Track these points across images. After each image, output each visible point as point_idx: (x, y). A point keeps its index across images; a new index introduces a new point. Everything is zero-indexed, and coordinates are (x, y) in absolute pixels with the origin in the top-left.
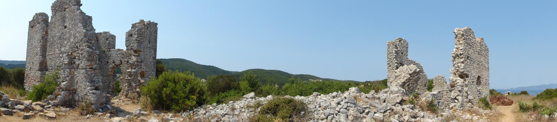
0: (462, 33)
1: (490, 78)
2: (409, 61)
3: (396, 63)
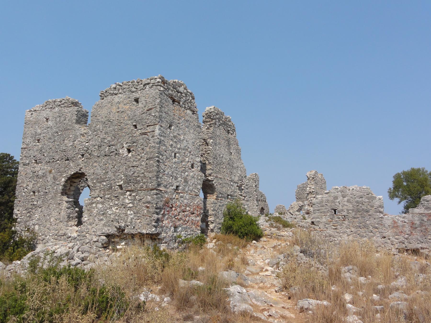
0: (313, 177)
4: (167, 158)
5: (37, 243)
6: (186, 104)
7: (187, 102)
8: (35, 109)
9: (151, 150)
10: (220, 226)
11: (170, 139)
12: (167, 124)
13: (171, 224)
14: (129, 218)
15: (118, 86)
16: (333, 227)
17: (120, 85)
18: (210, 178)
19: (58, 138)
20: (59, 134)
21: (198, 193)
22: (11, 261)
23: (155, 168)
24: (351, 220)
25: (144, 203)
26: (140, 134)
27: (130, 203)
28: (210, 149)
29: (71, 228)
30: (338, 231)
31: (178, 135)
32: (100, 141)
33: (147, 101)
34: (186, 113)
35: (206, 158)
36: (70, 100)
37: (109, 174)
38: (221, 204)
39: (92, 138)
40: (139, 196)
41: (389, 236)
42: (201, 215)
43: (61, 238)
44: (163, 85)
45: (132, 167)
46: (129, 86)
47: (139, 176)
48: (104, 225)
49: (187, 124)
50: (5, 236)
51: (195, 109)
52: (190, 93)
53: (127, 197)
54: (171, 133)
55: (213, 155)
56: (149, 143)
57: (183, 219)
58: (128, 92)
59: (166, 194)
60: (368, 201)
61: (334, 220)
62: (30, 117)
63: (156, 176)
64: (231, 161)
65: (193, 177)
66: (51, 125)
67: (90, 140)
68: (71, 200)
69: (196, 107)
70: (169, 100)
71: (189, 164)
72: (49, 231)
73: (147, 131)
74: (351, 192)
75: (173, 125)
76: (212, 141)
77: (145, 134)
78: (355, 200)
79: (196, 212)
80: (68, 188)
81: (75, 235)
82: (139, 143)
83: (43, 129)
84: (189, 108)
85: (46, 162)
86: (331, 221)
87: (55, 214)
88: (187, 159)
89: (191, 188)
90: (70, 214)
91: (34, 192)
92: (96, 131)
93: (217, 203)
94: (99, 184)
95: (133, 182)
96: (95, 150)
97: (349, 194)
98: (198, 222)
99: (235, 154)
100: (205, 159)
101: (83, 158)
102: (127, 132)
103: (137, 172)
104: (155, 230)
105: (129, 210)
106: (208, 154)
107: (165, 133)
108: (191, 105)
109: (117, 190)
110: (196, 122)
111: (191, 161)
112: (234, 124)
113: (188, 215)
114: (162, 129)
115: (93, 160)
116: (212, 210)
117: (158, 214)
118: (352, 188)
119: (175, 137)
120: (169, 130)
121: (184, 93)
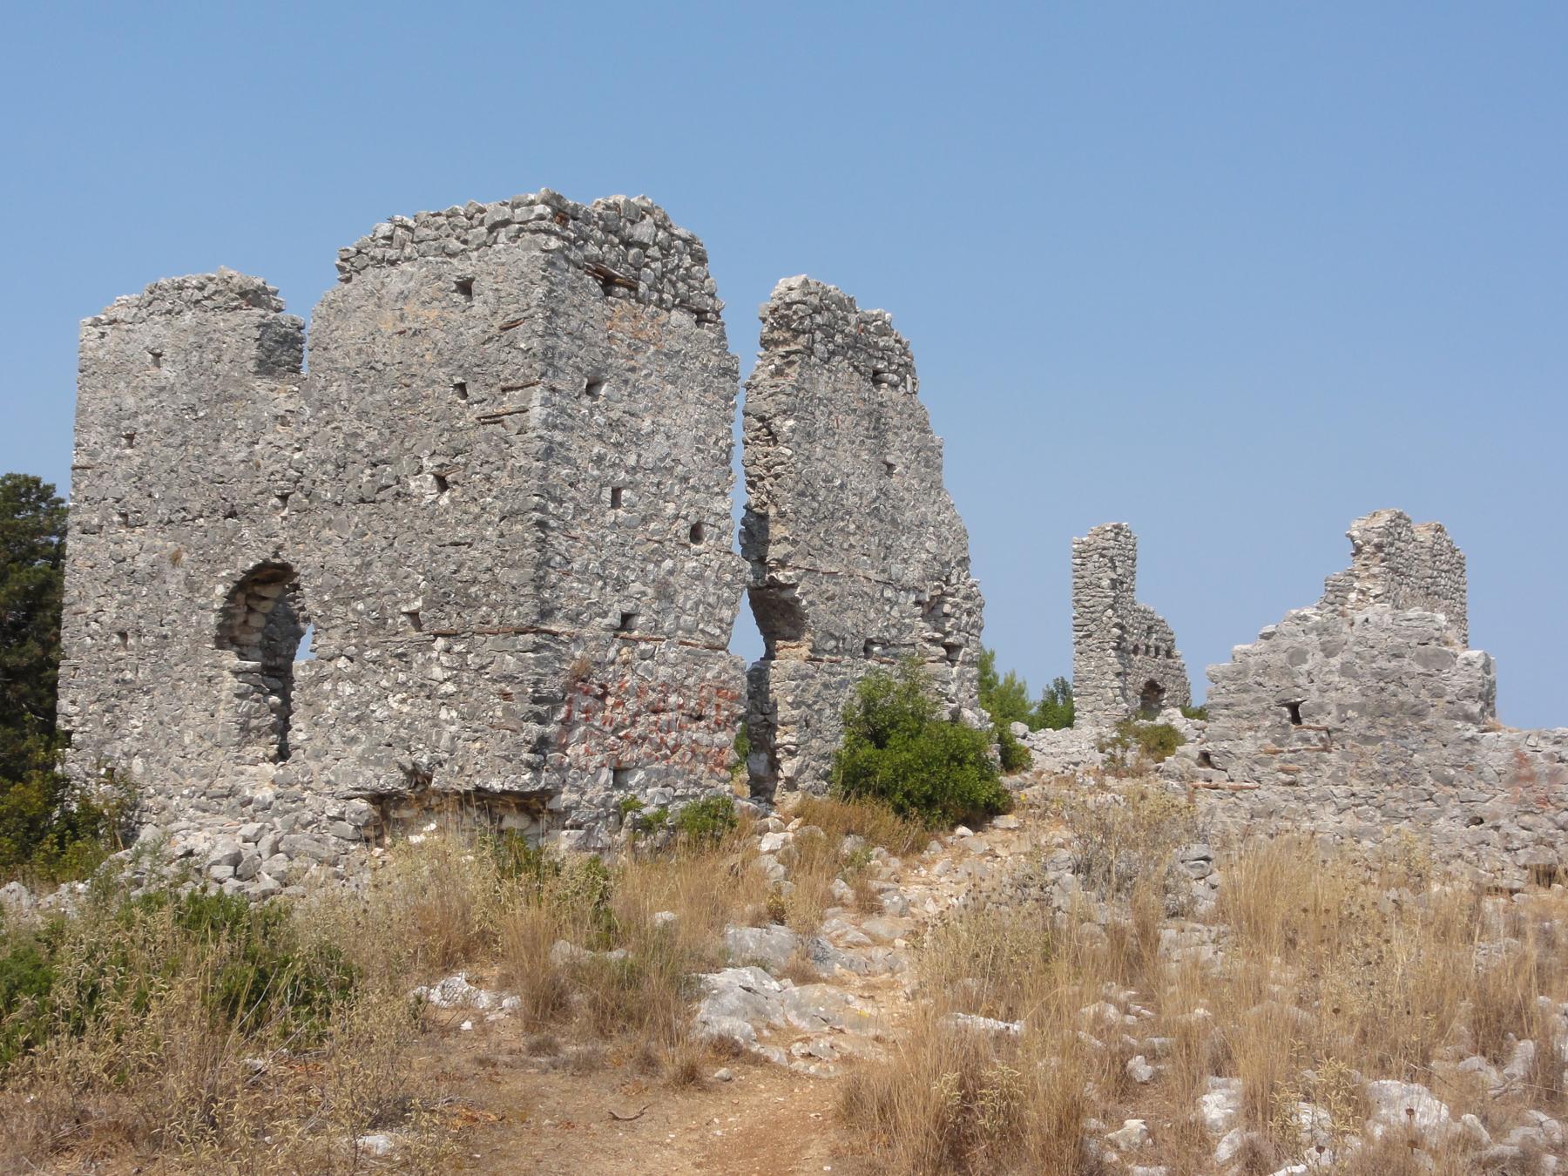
0: (1376, 540)
1: (1499, 704)
2: (1139, 611)
3: (1116, 625)
4: (579, 510)
5: (141, 824)
6: (667, 286)
7: (670, 281)
8: (112, 315)
9: (516, 482)
10: (828, 767)
11: (592, 435)
12: (577, 380)
13: (599, 758)
14: (446, 736)
15: (399, 232)
16: (1283, 776)
17: (407, 228)
18: (781, 576)
19: (198, 430)
20: (201, 414)
21: (724, 638)
22: (54, 882)
23: (530, 550)
24: (1354, 750)
25: (494, 681)
26: (479, 419)
27: (448, 679)
28: (785, 459)
29: (252, 769)
30: (1300, 791)
31: (627, 417)
32: (340, 443)
33: (503, 294)
34: (664, 325)
35: (769, 492)
36: (235, 281)
37: (373, 572)
38: (833, 680)
39: (315, 433)
40: (477, 655)
41: (1496, 816)
42: (734, 723)
43: (220, 804)
44: (557, 228)
45: (451, 544)
46: (437, 229)
47: (475, 581)
48: (363, 760)
49: (668, 370)
50: (31, 796)
51: (710, 301)
52: (685, 241)
53: (438, 659)
54: (597, 413)
55: (797, 483)
56: (507, 454)
57: (651, 740)
58: (435, 256)
59: (578, 648)
60: (1422, 670)
61: (1285, 749)
62: (98, 348)
63: (533, 580)
64: (888, 499)
65: (699, 577)
66: (172, 381)
67: (307, 440)
68: (250, 664)
69: (712, 295)
70: (585, 281)
71: (682, 528)
72: (180, 780)
73: (500, 410)
74: (1357, 633)
75: (607, 380)
76: (791, 423)
77: (495, 419)
78: (1374, 665)
79: (713, 713)
80: (240, 619)
81: (266, 793)
82: (476, 453)
83: (142, 394)
84: (682, 301)
85: (160, 522)
86: (1276, 753)
87: (195, 716)
88: (671, 508)
89: (687, 619)
90: (248, 715)
91: (123, 635)
92: (326, 406)
93: (813, 677)
94: (340, 609)
95: (456, 603)
96: (325, 477)
97: (1352, 639)
98: (721, 751)
99: (907, 467)
100: (764, 497)
101: (284, 508)
102: (434, 412)
103: (470, 563)
104: (531, 779)
105: (444, 704)
106: (777, 476)
107: (570, 416)
108: (690, 287)
109: (405, 632)
110: (714, 354)
111: (687, 515)
112: (904, 340)
113: (673, 724)
114: (556, 399)
115: (319, 518)
116: (789, 704)
117: (541, 720)
118: (1364, 617)
119: (612, 425)
120: (586, 401)
121: (655, 244)
